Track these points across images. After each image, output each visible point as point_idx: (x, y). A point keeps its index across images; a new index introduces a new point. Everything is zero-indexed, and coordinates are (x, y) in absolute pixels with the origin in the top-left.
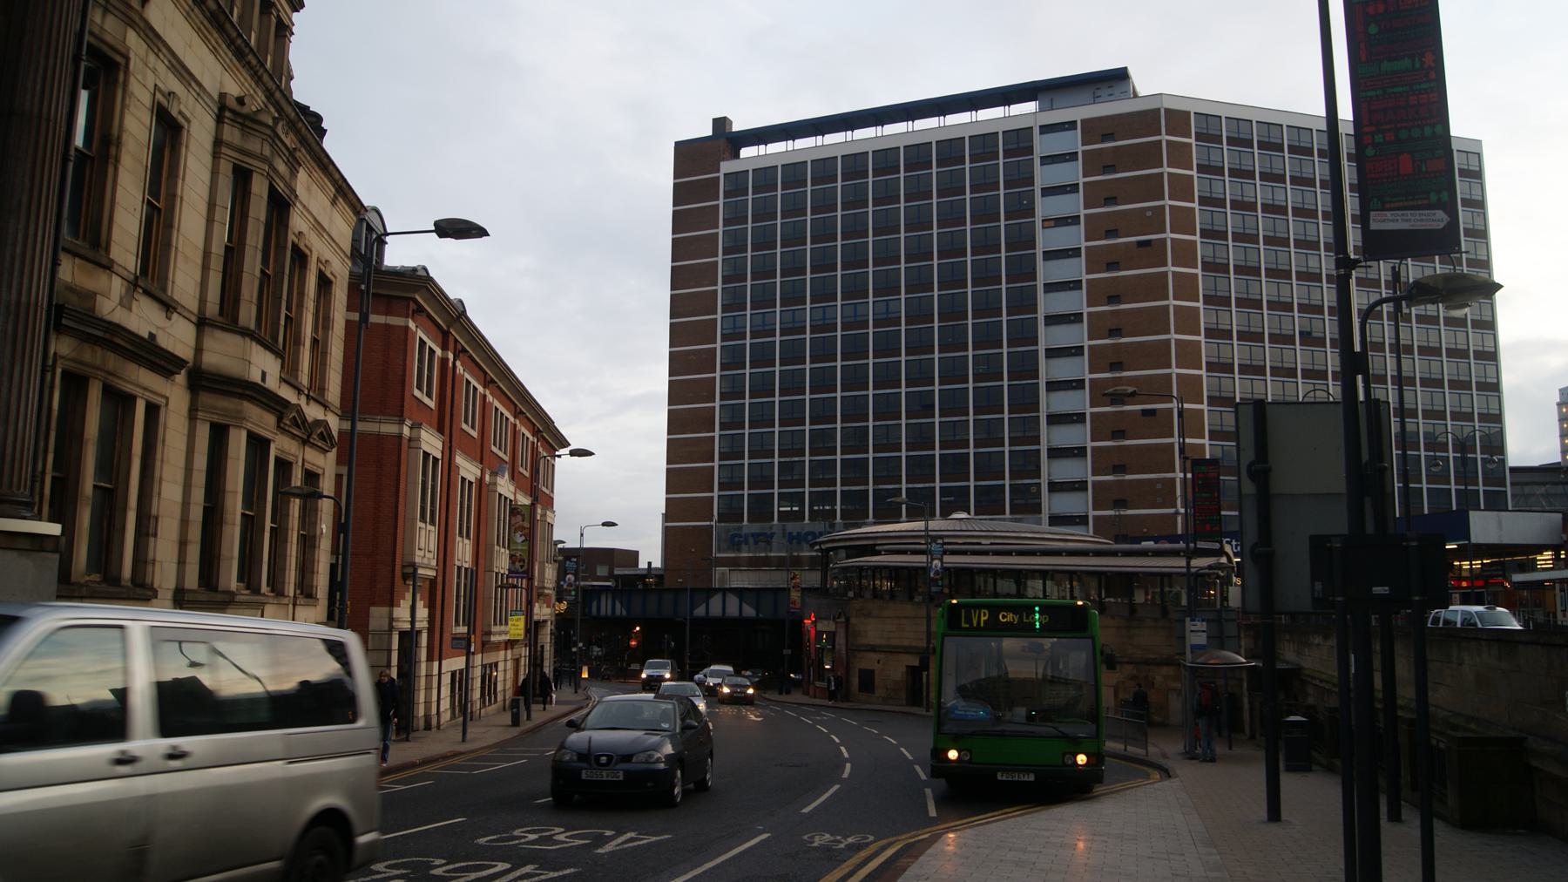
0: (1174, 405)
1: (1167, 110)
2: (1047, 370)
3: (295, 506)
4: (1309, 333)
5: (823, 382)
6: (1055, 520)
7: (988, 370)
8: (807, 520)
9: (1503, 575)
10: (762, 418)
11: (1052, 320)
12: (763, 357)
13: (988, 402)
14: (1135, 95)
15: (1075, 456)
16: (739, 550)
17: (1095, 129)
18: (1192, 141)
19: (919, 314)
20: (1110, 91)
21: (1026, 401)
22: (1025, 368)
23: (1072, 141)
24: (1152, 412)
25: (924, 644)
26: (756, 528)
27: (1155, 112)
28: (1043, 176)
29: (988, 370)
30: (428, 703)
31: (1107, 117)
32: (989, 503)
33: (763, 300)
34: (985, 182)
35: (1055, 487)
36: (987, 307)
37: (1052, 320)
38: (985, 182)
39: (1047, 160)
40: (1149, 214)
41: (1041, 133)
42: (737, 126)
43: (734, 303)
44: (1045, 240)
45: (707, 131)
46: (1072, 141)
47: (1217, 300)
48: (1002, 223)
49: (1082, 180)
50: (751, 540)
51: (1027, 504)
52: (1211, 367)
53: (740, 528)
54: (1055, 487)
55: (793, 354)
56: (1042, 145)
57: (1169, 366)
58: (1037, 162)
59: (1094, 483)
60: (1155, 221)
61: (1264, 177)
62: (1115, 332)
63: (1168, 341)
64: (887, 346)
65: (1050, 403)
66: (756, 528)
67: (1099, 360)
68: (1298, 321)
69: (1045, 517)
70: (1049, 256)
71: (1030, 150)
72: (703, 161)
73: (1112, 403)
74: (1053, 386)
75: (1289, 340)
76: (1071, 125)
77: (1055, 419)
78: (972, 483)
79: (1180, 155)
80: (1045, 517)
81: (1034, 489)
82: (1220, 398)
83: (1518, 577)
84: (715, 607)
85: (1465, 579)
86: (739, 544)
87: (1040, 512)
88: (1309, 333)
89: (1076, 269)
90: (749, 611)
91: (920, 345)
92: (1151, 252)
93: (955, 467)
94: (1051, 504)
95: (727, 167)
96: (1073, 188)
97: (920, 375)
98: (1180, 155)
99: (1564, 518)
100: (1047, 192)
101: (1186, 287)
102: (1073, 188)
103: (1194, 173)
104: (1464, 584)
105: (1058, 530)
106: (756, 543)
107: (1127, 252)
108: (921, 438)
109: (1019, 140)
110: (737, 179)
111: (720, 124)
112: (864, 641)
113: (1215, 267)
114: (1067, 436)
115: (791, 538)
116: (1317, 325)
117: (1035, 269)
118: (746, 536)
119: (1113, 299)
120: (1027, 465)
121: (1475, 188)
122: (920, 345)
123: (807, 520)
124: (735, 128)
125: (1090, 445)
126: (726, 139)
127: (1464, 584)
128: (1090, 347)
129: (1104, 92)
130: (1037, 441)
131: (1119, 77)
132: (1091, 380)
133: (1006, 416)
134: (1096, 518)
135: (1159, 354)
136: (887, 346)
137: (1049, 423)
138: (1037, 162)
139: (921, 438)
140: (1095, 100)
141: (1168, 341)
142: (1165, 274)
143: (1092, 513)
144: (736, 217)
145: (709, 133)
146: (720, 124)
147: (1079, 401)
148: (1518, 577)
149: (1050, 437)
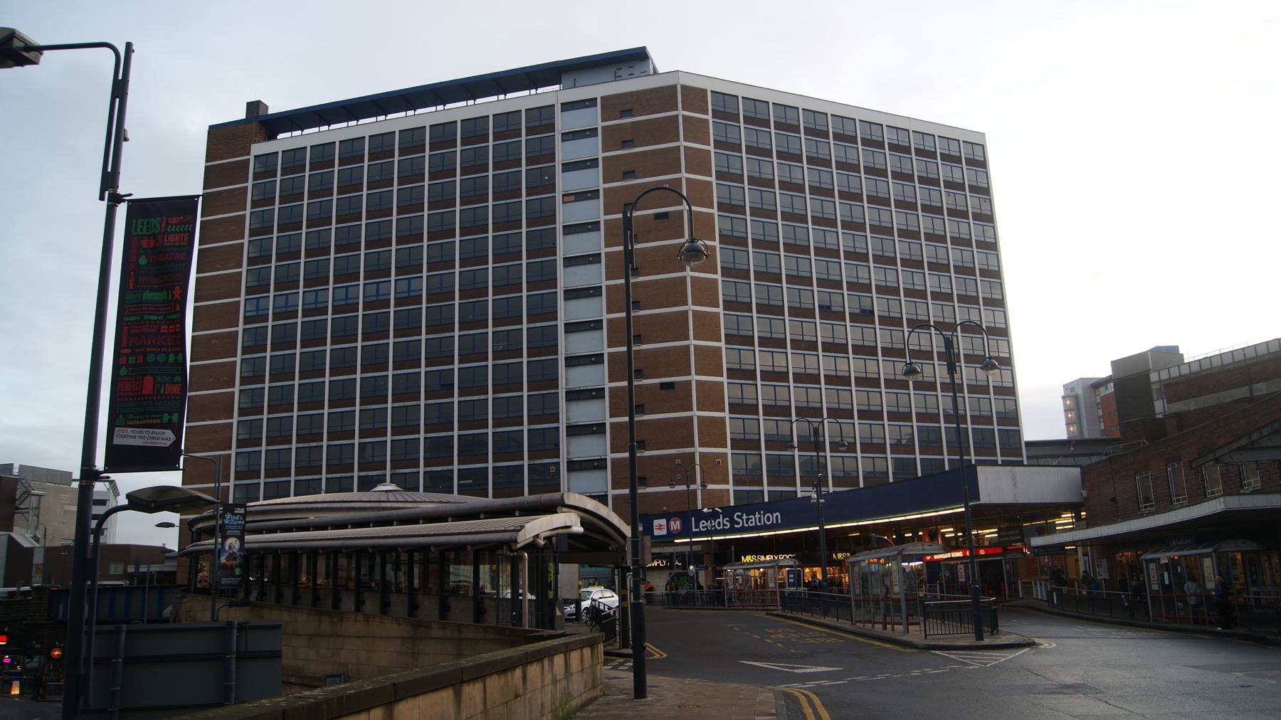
0: (685, 207)
1: (683, 87)
4: (829, 308)
5: (343, 364)
7: (508, 348)
9: (1022, 541)
10: (281, 402)
12: (284, 340)
13: (508, 380)
14: (655, 72)
15: (594, 433)
17: (614, 106)
18: (709, 117)
19: (440, 293)
20: (631, 71)
21: (545, 378)
22: (545, 344)
23: (592, 118)
24: (670, 386)
28: (564, 152)
29: (508, 348)
31: (626, 94)
33: (286, 282)
34: (507, 160)
36: (507, 284)
37: (572, 294)
38: (507, 160)
39: (569, 136)
41: (563, 171)
42: (274, 108)
43: (258, 287)
44: (565, 214)
45: (241, 114)
47: (740, 339)
48: (524, 199)
49: (601, 155)
52: (734, 408)
55: (314, 336)
56: (563, 122)
57: (686, 303)
58: (558, 138)
60: (679, 361)
61: (781, 155)
63: (688, 347)
64: (408, 326)
65: (568, 378)
68: (816, 295)
70: (569, 230)
71: (551, 127)
73: (624, 179)
74: (572, 361)
75: (810, 313)
76: (592, 102)
79: (696, 130)
82: (741, 370)
83: (1037, 541)
85: (984, 547)
88: (829, 308)
91: (440, 324)
92: (675, 395)
93: (473, 449)
96: (593, 163)
97: (440, 355)
98: (696, 130)
99: (1083, 473)
100: (568, 167)
101: (707, 327)
102: (593, 163)
103: (711, 148)
104: (982, 552)
108: (440, 420)
109: (542, 119)
111: (254, 108)
113: (735, 272)
116: (836, 300)
117: (555, 244)
121: (999, 315)
122: (440, 324)
126: (262, 122)
127: (982, 552)
128: (609, 321)
129: (625, 72)
131: (637, 57)
133: (525, 393)
135: (677, 327)
136: (408, 326)
138: (558, 138)
139: (440, 420)
140: (617, 78)
141: (688, 347)
144: (264, 199)
146: (254, 108)
148: (1037, 541)
149: (569, 414)
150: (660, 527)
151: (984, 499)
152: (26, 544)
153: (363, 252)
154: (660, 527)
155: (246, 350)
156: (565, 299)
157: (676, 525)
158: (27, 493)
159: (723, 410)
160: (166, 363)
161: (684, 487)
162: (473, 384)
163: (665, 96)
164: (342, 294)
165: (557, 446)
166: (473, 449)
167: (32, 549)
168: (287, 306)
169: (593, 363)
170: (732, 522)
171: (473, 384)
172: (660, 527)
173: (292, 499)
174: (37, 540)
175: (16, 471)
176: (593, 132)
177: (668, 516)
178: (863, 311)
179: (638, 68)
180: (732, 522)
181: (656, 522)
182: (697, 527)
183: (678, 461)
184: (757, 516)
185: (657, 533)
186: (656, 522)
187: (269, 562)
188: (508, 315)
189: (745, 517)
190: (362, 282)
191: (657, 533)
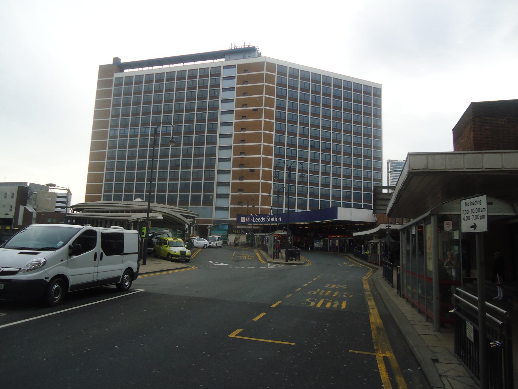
1: (267, 62)
3: (173, 258)
6: (218, 208)
11: (223, 124)
17: (243, 68)
20: (249, 55)
22: (211, 154)
23: (234, 72)
24: (253, 171)
35: (218, 196)
36: (200, 131)
39: (225, 78)
40: (258, 99)
49: (236, 86)
51: (208, 201)
54: (218, 196)
56: (224, 73)
58: (221, 79)
59: (232, 195)
60: (259, 102)
62: (243, 141)
67: (237, 150)
72: (112, 75)
76: (233, 66)
77: (222, 136)
78: (190, 194)
81: (211, 197)
89: (232, 95)
95: (117, 75)
107: (248, 112)
109: (216, 72)
110: (119, 79)
111: (116, 60)
114: (224, 178)
119: (243, 129)
120: (209, 188)
124: (122, 61)
125: (231, 181)
126: (118, 66)
129: (247, 55)
130: (213, 179)
131: (250, 51)
133: (204, 170)
137: (217, 185)
138: (221, 79)
140: (244, 58)
143: (230, 206)
145: (84, 202)
146: (116, 60)
147: (231, 130)
151: (338, 219)
152: (30, 211)
153: (141, 117)
154: (243, 219)
155: (109, 148)
158: (32, 193)
161: (246, 206)
162: (186, 166)
163: (259, 66)
164: (165, 129)
166: (173, 189)
167: (32, 213)
168: (124, 133)
170: (266, 219)
171: (186, 166)
173: (112, 201)
174: (35, 209)
175: (28, 185)
176: (233, 77)
177: (246, 216)
178: (327, 148)
180: (266, 219)
181: (242, 218)
183: (254, 197)
185: (242, 221)
186: (242, 218)
188: (200, 142)
190: (129, 128)
191: (242, 221)
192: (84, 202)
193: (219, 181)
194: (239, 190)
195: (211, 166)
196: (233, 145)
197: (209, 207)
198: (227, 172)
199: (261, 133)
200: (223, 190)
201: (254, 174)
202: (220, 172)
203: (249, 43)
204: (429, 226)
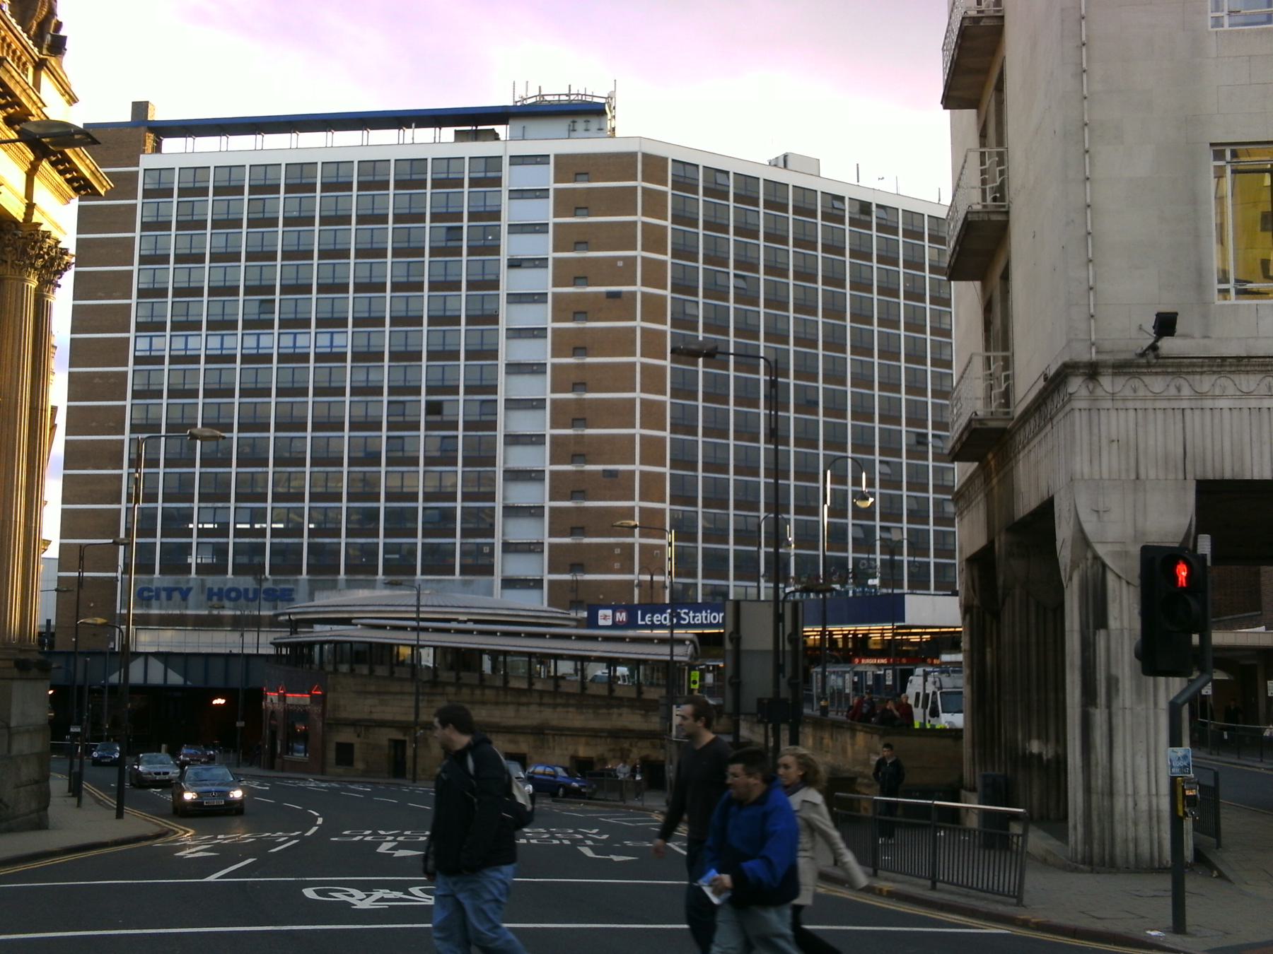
1: (645, 155)
2: (505, 423)
6: (509, 583)
8: (157, 574)
16: (149, 606)
17: (569, 166)
23: (545, 177)
25: (412, 718)
26: (169, 581)
27: (632, 156)
30: (1102, 830)
32: (400, 568)
40: (620, 264)
42: (158, 114)
45: (125, 116)
46: (545, 177)
49: (551, 255)
50: (163, 595)
51: (479, 565)
53: (151, 581)
54: (508, 548)
56: (511, 178)
58: (505, 195)
66: (169, 581)
67: (562, 414)
69: (497, 579)
76: (542, 159)
80: (497, 579)
84: (136, 674)
86: (149, 599)
87: (492, 573)
90: (175, 679)
94: (505, 565)
105: (509, 593)
106: (169, 598)
107: (588, 304)
111: (140, 108)
112: (344, 715)
114: (524, 494)
115: (210, 594)
118: (158, 590)
119: (579, 350)
120: (480, 525)
123: (157, 574)
125: (548, 504)
129: (580, 124)
130: (491, 497)
131: (587, 112)
132: (554, 294)
134: (551, 583)
138: (505, 195)
141: (633, 436)
142: (633, 330)
143: (547, 577)
145: (129, 119)
146: (140, 108)
150: (605, 617)
156: (507, 373)
157: (622, 617)
159: (664, 501)
160: (817, 593)
163: (622, 163)
165: (492, 525)
169: (533, 443)
172: (605, 617)
179: (594, 123)
181: (601, 612)
182: (643, 619)
184: (704, 614)
186: (601, 612)
187: (317, 648)
189: (691, 614)
192: (129, 119)
193: (511, 502)
194: (575, 349)
195: (482, 457)
196: (549, 396)
197: (482, 579)
198: (536, 369)
199: (635, 223)
200: (523, 531)
201: (619, 304)
202: (514, 475)
203: (592, 87)
204: (1098, 711)
